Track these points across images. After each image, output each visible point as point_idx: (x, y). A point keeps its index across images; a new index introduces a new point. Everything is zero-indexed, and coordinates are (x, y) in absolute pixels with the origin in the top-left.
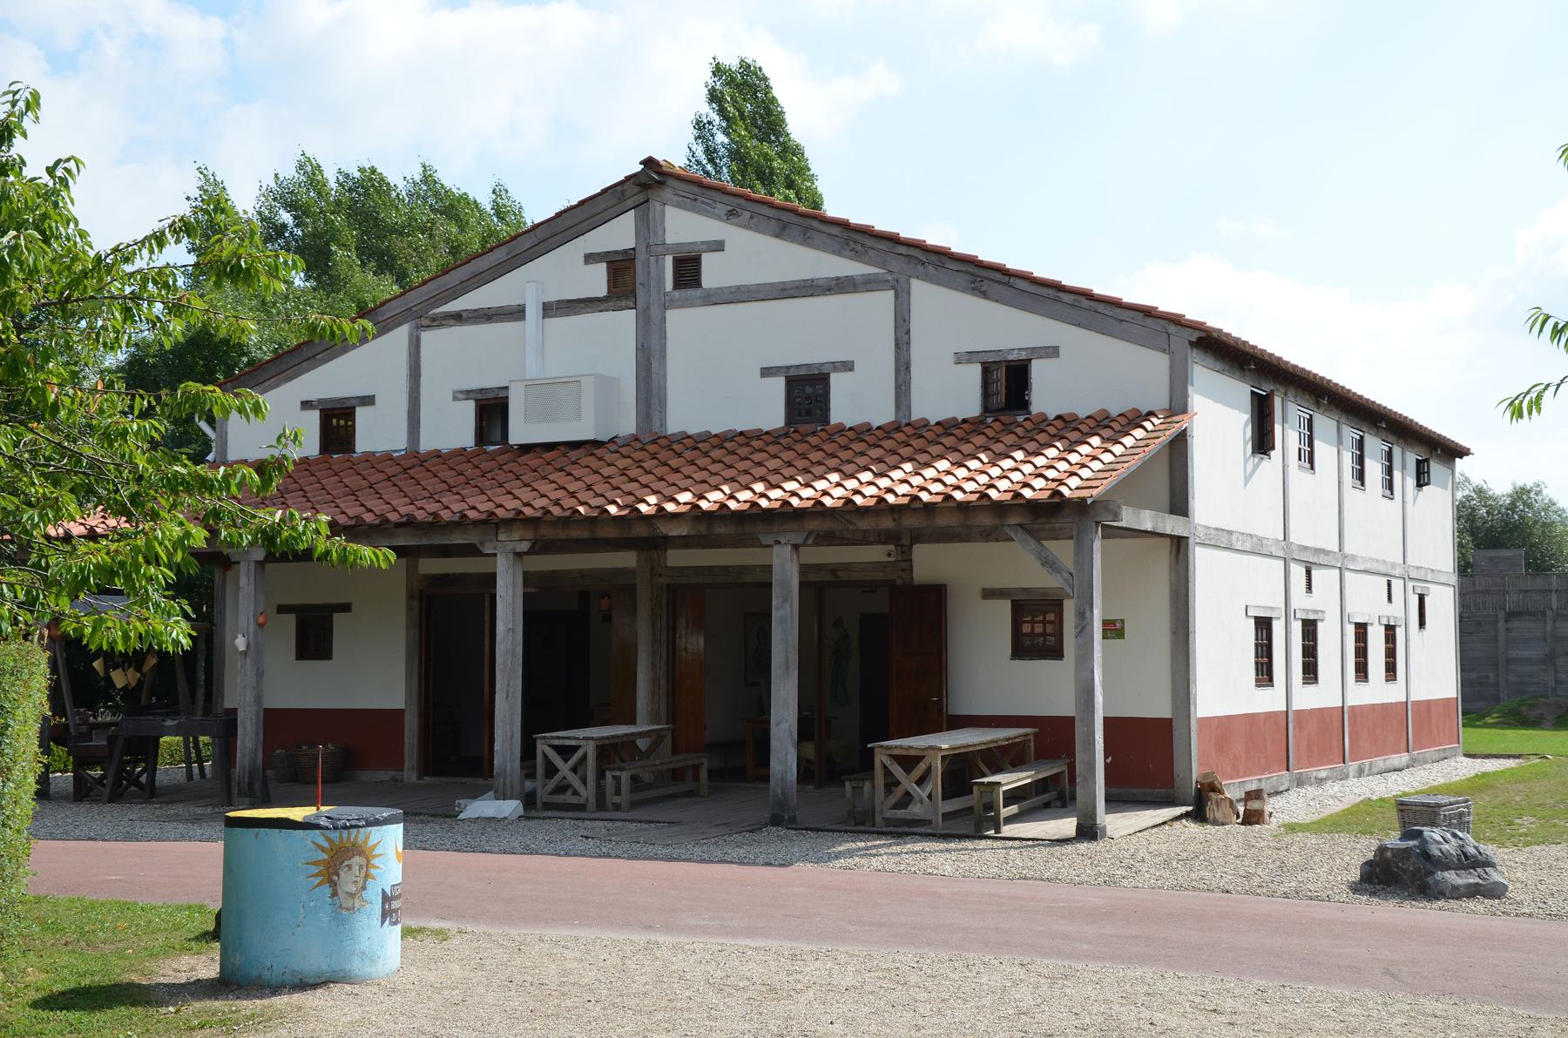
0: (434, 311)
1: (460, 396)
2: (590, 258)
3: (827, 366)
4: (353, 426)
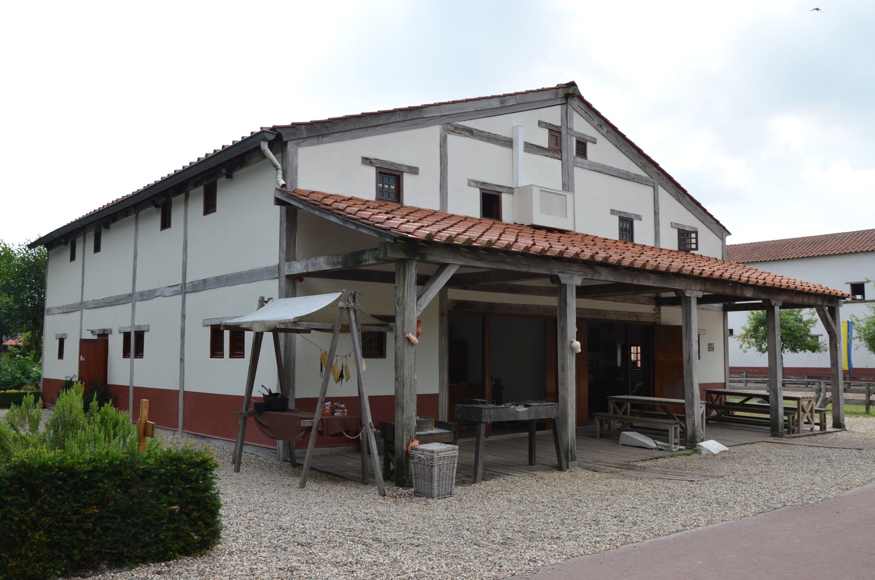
0: (456, 123)
1: (472, 183)
2: (541, 124)
3: (633, 215)
4: (377, 182)
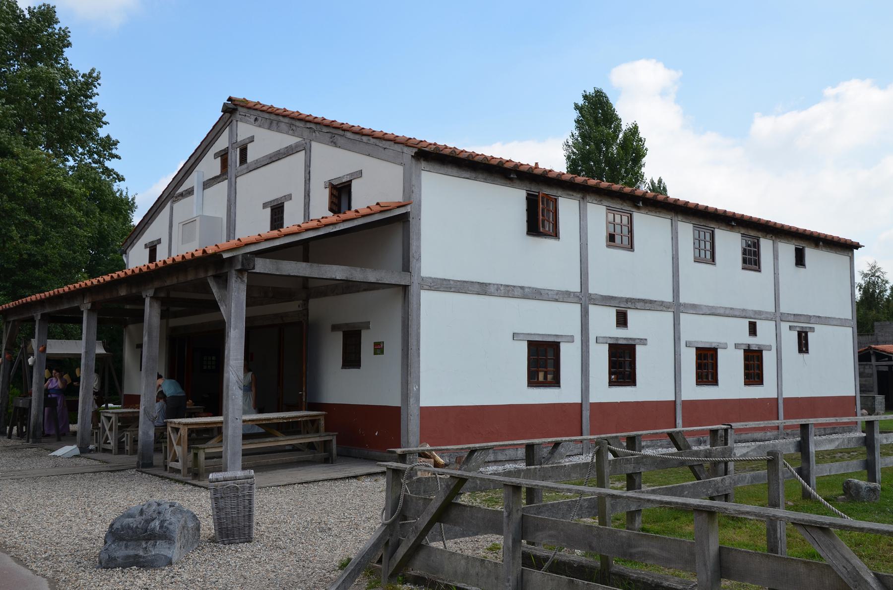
0: (177, 192)
